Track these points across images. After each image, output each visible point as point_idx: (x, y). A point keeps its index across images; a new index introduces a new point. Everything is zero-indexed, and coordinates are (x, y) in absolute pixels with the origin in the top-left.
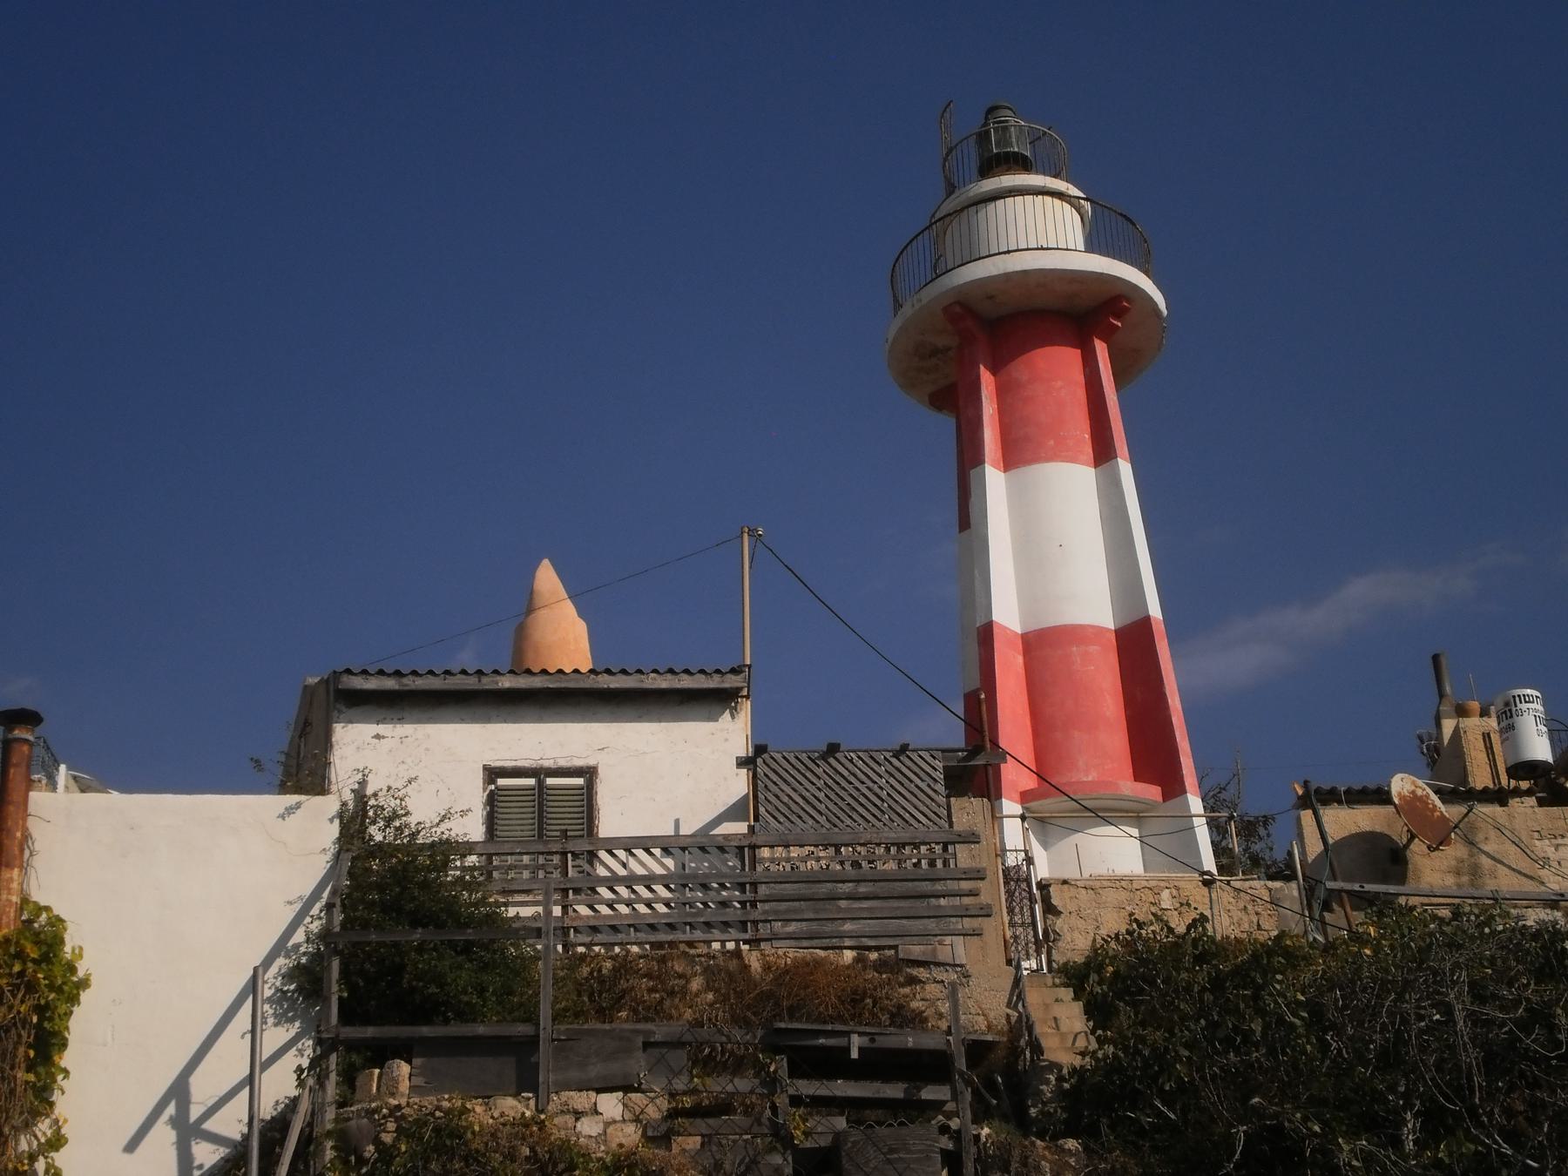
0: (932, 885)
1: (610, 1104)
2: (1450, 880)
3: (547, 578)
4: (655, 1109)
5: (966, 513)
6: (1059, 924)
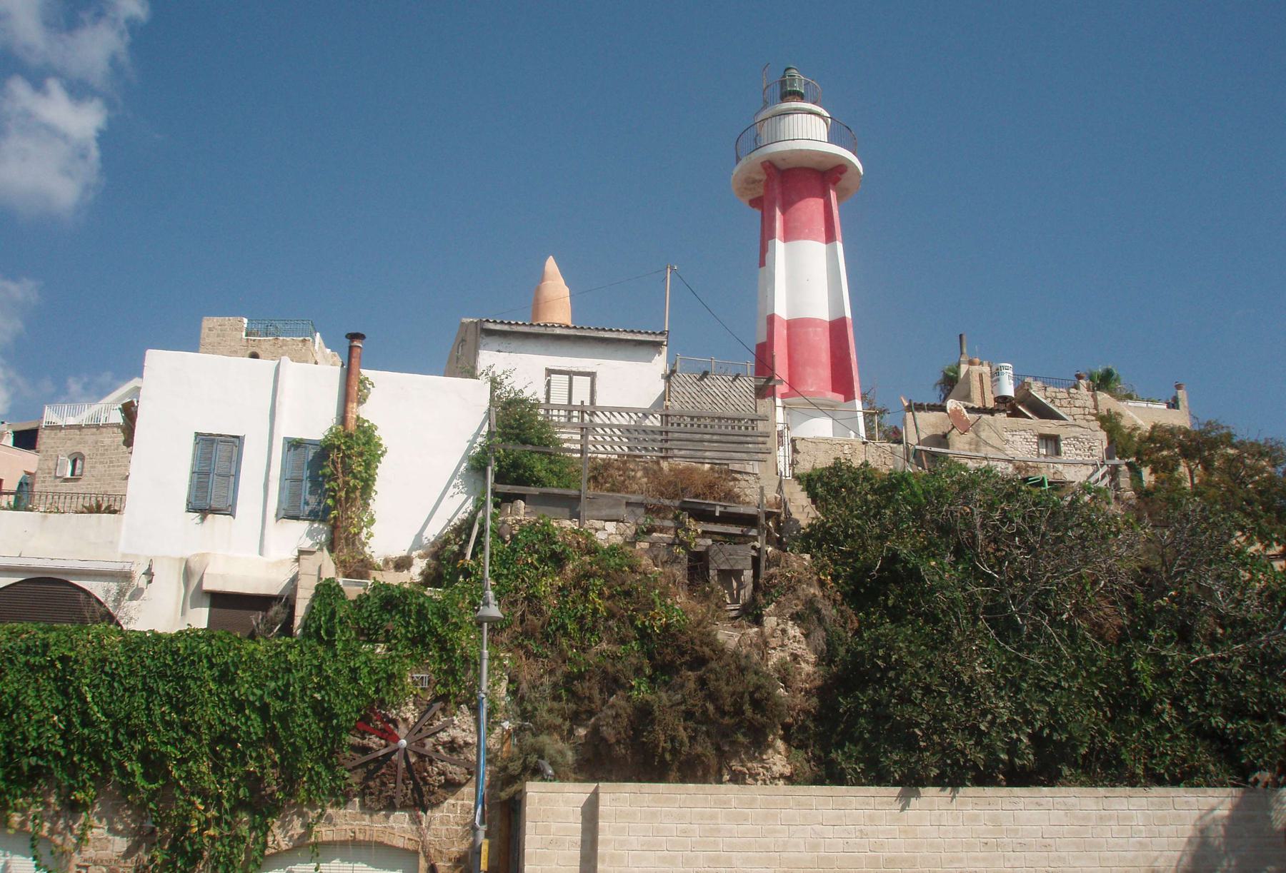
0: (745, 435)
1: (611, 527)
2: (967, 447)
3: (551, 265)
4: (630, 532)
5: (763, 256)
6: (799, 457)
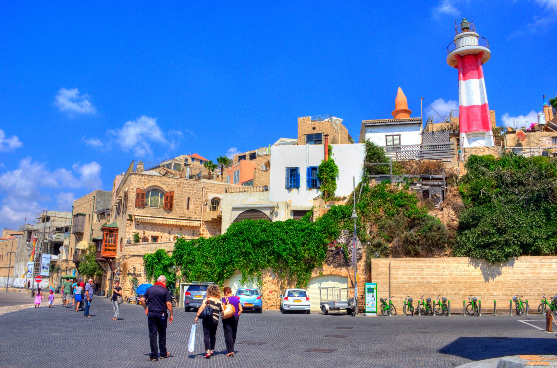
3: (400, 90)
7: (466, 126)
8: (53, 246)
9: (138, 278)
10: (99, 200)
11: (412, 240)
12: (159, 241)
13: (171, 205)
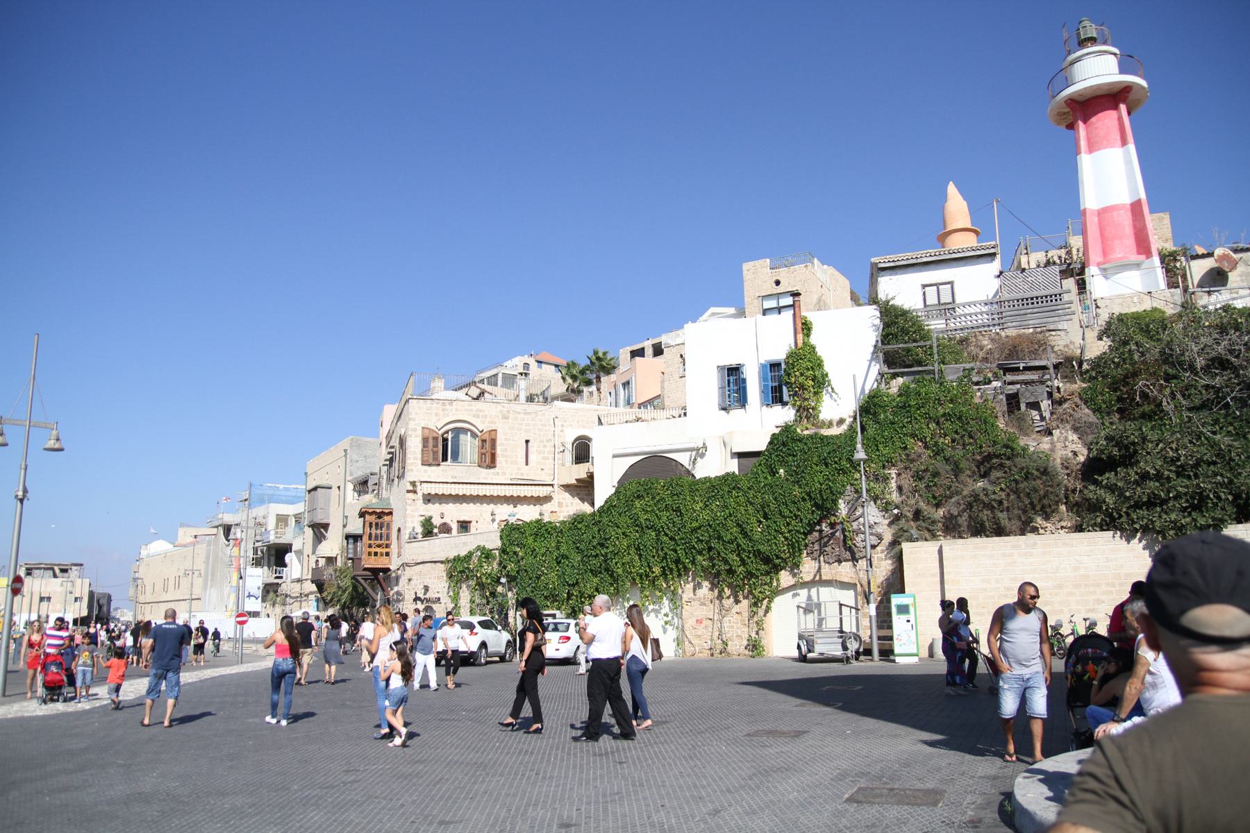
3: (952, 189)
7: (1100, 252)
8: (273, 552)
9: (435, 606)
10: (355, 457)
11: (986, 500)
12: (473, 530)
13: (493, 456)
